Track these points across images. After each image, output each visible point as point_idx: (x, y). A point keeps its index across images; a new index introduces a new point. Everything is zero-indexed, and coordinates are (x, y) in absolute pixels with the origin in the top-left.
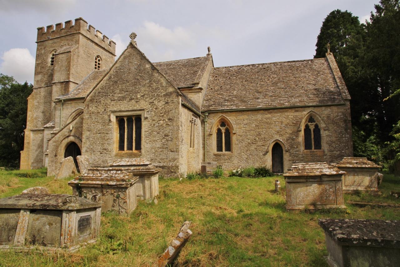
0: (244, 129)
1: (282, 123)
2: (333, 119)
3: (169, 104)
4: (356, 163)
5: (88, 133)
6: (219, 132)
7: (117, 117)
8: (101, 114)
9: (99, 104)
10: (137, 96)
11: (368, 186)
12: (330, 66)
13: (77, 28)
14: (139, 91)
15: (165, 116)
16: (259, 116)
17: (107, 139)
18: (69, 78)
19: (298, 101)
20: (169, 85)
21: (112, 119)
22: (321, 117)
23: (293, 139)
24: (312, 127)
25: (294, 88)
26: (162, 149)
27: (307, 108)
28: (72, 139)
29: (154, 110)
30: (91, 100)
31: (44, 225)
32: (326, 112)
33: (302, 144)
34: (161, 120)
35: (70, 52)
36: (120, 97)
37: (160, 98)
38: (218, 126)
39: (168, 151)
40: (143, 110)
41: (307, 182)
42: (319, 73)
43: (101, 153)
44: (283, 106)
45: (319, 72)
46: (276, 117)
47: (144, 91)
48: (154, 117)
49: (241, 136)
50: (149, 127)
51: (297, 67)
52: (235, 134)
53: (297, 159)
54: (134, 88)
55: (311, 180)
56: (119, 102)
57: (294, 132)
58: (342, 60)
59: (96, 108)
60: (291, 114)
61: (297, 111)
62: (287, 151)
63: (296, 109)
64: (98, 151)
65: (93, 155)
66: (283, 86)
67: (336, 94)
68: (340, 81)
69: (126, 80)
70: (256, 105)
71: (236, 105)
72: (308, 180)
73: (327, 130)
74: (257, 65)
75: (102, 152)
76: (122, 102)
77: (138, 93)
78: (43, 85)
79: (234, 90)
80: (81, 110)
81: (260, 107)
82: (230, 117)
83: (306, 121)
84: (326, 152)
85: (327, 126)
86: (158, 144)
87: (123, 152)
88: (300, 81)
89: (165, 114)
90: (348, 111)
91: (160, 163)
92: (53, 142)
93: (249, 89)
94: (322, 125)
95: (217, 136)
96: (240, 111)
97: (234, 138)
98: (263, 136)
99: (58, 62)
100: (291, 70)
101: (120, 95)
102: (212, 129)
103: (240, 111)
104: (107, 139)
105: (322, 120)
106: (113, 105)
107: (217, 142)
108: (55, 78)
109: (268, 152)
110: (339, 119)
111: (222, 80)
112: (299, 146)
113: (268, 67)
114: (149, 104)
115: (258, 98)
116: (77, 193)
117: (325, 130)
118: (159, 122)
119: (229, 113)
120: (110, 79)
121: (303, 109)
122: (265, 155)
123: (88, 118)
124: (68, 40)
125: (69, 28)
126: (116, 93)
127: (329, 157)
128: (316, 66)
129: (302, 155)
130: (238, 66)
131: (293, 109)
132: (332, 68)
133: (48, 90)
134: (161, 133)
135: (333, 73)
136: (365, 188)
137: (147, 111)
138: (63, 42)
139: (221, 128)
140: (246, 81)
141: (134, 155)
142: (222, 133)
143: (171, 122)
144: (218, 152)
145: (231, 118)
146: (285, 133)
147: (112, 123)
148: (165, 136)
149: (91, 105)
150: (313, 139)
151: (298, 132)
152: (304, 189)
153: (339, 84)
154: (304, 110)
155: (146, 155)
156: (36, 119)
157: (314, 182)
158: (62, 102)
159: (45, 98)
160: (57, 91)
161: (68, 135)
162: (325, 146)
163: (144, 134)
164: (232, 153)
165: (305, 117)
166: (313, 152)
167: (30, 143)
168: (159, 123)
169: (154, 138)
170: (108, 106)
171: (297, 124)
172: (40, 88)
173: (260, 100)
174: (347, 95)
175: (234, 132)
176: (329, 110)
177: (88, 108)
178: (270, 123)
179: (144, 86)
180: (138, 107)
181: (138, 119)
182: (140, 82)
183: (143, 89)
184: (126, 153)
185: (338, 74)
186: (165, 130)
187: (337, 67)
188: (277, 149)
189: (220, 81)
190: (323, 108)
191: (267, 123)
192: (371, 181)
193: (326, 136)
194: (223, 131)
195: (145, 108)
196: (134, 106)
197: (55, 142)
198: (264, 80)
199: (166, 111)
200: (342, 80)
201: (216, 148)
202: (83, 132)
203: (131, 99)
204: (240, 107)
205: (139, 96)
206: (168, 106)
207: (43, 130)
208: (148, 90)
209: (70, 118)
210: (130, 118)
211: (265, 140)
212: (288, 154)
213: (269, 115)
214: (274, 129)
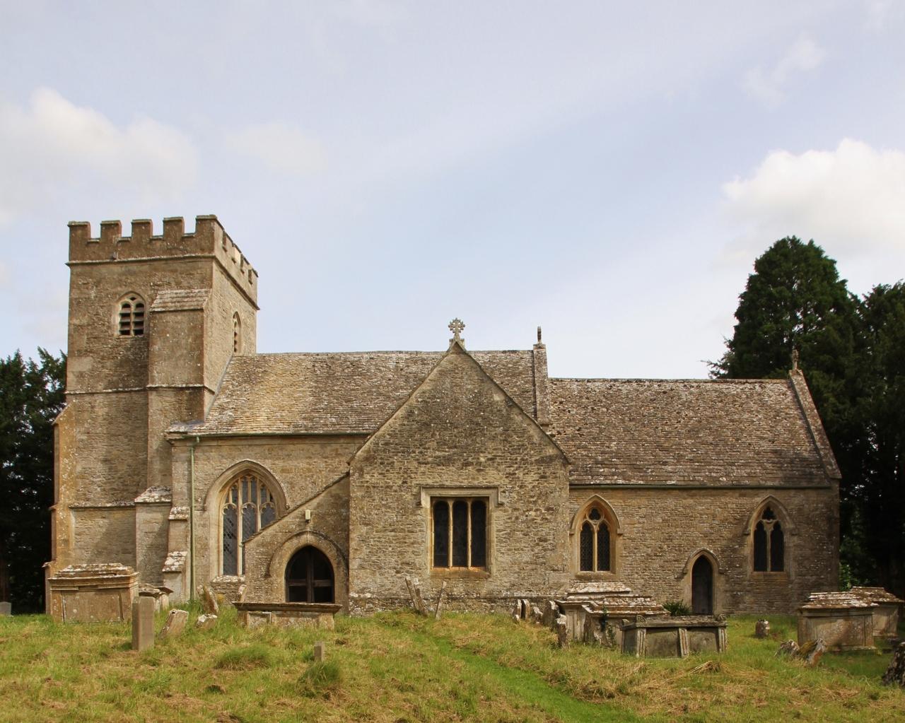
0: (641, 525)
1: (714, 517)
2: (809, 514)
3: (548, 479)
4: (871, 596)
5: (364, 529)
6: (587, 528)
7: (432, 498)
8: (396, 491)
9: (387, 468)
10: (478, 458)
11: (884, 630)
12: (799, 401)
13: (205, 244)
14: (483, 449)
15: (540, 501)
16: (670, 502)
17: (413, 544)
18: (201, 380)
19: (745, 475)
20: (545, 441)
21: (423, 503)
22: (786, 510)
23: (734, 551)
24: (769, 529)
25: (734, 446)
26: (534, 566)
27: (762, 491)
28: (308, 539)
29: (517, 488)
30: (367, 459)
31: (701, 640)
32: (796, 500)
33: (749, 559)
34: (531, 510)
35: (202, 310)
36: (439, 457)
37: (529, 466)
38: (585, 517)
39: (546, 569)
40: (495, 488)
41: (831, 617)
42: (778, 416)
43: (398, 572)
44: (718, 485)
45: (778, 413)
46: (702, 505)
47: (494, 449)
48: (516, 503)
49: (633, 540)
50: (507, 522)
51: (733, 395)
52: (620, 535)
53: (738, 589)
54: (470, 442)
55: (836, 614)
56: (439, 468)
57: (735, 536)
58: (814, 380)
59: (380, 476)
60: (733, 502)
61: (744, 495)
62: (721, 573)
63: (743, 491)
64: (390, 568)
65: (378, 574)
66: (710, 439)
67: (814, 466)
68: (821, 438)
69: (451, 423)
70: (665, 478)
71: (623, 475)
72: (833, 614)
73: (796, 535)
74: (647, 383)
75: (401, 568)
76: (444, 468)
77: (482, 452)
78: (100, 387)
79: (610, 440)
80: (249, 464)
81: (673, 482)
82: (611, 501)
83: (758, 516)
84: (793, 578)
85: (796, 528)
86: (526, 557)
87: (447, 569)
88: (742, 431)
89: (539, 498)
90: (836, 500)
91: (530, 591)
92: (258, 546)
93: (641, 441)
94: (788, 525)
95: (581, 538)
96: (632, 489)
97: (619, 545)
98: (676, 542)
99: (164, 332)
100: (721, 401)
101: (438, 453)
102: (574, 524)
103: (632, 489)
104: (413, 544)
105: (790, 515)
106: (424, 473)
107: (581, 551)
108: (155, 374)
109: (686, 574)
110: (818, 514)
111: (577, 413)
112: (744, 564)
113: (672, 390)
114: (507, 477)
115: (665, 463)
116: (599, 627)
117: (793, 535)
118: (527, 513)
119: (610, 491)
120: (409, 415)
121: (756, 492)
122: (679, 579)
123: (363, 497)
124: (175, 271)
125: (179, 238)
126: (429, 448)
127: (796, 586)
128: (770, 397)
129: (749, 581)
130: (604, 380)
131: (738, 491)
132: (804, 406)
133: (118, 401)
134: (532, 535)
135: (806, 418)
136: (880, 633)
137: (502, 490)
138: (159, 274)
139: (591, 521)
140: (630, 420)
141: (473, 575)
142: (591, 533)
143: (551, 514)
144: (585, 572)
145: (614, 503)
146: (718, 537)
147: (424, 510)
148: (540, 540)
149: (369, 468)
150: (769, 550)
151: (744, 537)
152: (827, 625)
153: (818, 444)
154: (756, 495)
155: (501, 576)
156: (83, 478)
157: (838, 617)
158: (196, 441)
159: (110, 423)
160: (163, 411)
161: (297, 530)
162: (791, 565)
163: (495, 536)
164: (614, 573)
165: (759, 508)
166: (770, 575)
167: (70, 541)
168: (527, 516)
169: (518, 544)
170: (413, 475)
171: (741, 521)
172: (92, 394)
173: (669, 468)
174: (835, 470)
175: (619, 532)
176: (802, 496)
177: (361, 476)
178: (692, 517)
179: (493, 438)
180: (481, 481)
181: (480, 506)
182: (483, 429)
183: (490, 445)
184: (456, 573)
185: (816, 423)
186: (540, 529)
187: (813, 405)
188: (703, 568)
189: (573, 415)
190: (792, 493)
191: (686, 516)
192: (888, 622)
193: (794, 546)
194: (596, 528)
195: (496, 483)
196: (473, 479)
197: (263, 545)
198: (670, 420)
199: (541, 493)
200: (825, 437)
201: (579, 567)
202: (351, 527)
203: (467, 464)
204: (633, 481)
205: (482, 460)
206: (546, 484)
207: (134, 507)
208: (502, 448)
209: (217, 483)
210: (460, 503)
211: (680, 551)
212: (723, 578)
213: (690, 501)
214: (698, 529)
